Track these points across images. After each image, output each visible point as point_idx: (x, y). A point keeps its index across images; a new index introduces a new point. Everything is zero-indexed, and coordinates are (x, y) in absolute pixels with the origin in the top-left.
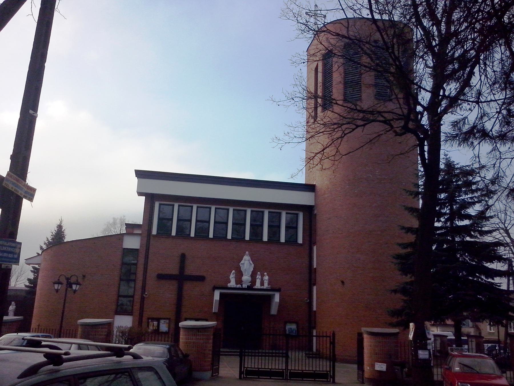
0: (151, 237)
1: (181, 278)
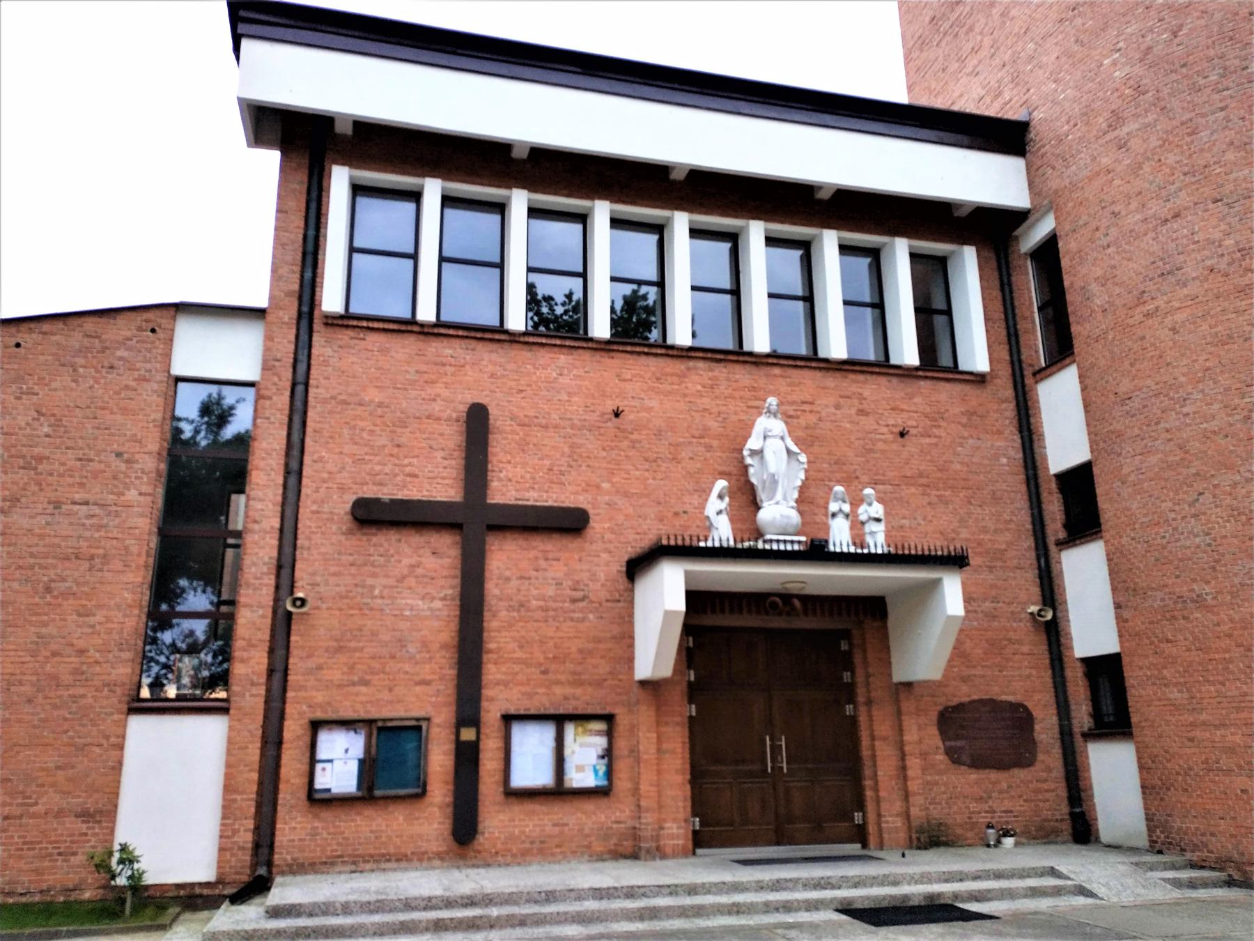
0: (317, 325)
1: (474, 522)
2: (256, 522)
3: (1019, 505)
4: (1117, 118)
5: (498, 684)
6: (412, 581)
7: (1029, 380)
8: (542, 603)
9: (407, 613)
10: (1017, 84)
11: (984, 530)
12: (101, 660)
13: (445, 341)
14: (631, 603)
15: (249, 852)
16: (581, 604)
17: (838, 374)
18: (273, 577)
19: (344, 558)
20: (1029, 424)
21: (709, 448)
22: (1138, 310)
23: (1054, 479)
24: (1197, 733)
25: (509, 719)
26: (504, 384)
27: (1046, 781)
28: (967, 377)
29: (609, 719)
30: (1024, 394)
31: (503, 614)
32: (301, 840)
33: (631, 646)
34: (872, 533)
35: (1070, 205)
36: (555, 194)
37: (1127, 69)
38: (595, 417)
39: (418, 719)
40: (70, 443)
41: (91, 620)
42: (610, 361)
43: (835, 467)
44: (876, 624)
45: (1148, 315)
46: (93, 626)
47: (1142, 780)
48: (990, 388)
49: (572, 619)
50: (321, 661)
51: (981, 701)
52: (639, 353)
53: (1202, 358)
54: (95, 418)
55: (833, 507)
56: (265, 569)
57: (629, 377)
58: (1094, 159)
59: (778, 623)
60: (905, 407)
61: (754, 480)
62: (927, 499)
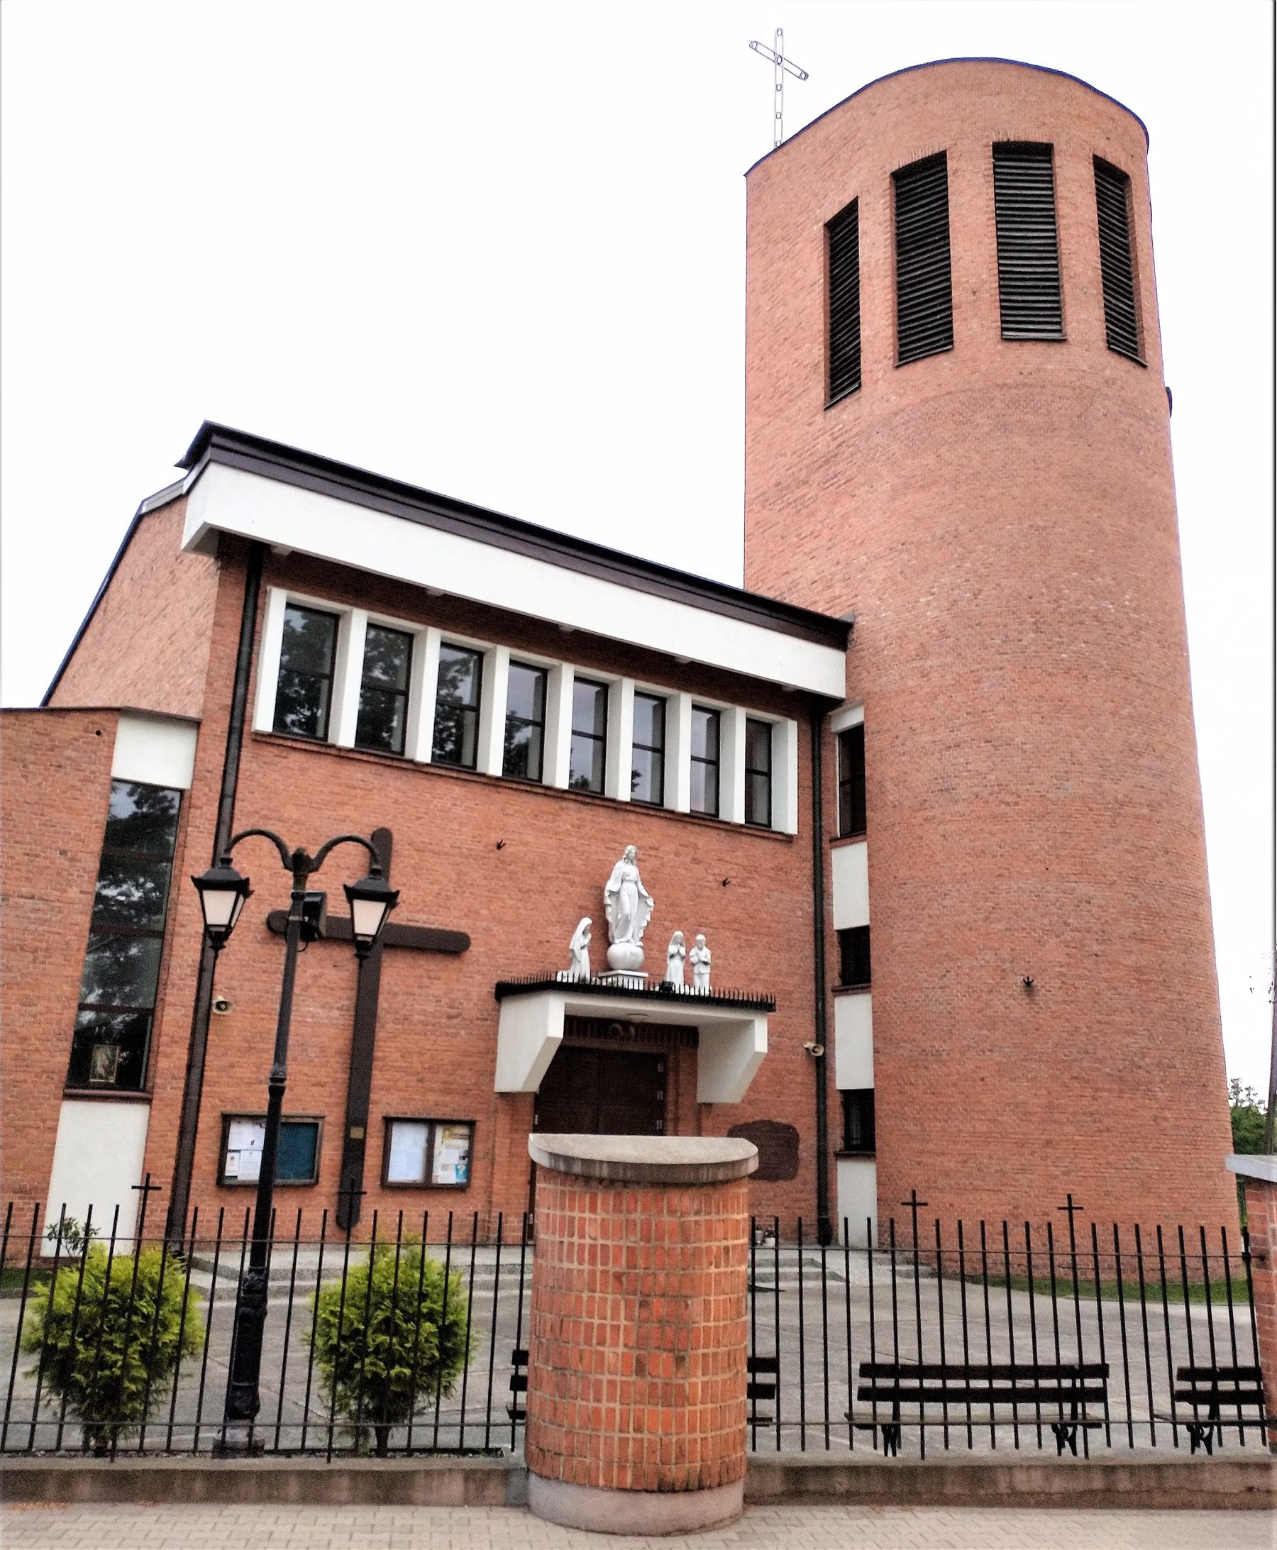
0: (246, 741)
2: (183, 926)
3: (807, 953)
4: (923, 652)
5: (382, 1089)
6: (314, 991)
7: (826, 845)
8: (422, 1018)
9: (309, 1020)
10: (847, 586)
11: (779, 973)
12: (41, 1048)
13: (358, 764)
14: (497, 1022)
15: (164, 1231)
16: (456, 1021)
17: (680, 825)
18: (195, 979)
19: (257, 965)
20: (822, 882)
21: (572, 883)
22: (920, 814)
23: (836, 935)
24: (924, 1159)
25: (389, 1122)
26: (405, 810)
27: (802, 1192)
28: (779, 837)
29: (471, 1124)
30: (821, 855)
31: (390, 1026)
32: (208, 1221)
33: (494, 1061)
34: (700, 974)
35: (879, 709)
36: (462, 633)
37: (937, 613)
38: (480, 847)
39: (315, 1118)
40: (18, 838)
41: (33, 1009)
42: (496, 796)
43: (670, 909)
44: (689, 1050)
45: (926, 820)
46: (35, 1016)
47: (879, 1193)
48: (795, 848)
49: (447, 1034)
50: (235, 1059)
51: (762, 1122)
52: (522, 791)
53: (961, 865)
54: (43, 815)
55: (672, 949)
56: (189, 971)
57: (511, 812)
58: (902, 678)
59: (614, 1045)
60: (728, 858)
61: (610, 918)
62: (738, 942)
